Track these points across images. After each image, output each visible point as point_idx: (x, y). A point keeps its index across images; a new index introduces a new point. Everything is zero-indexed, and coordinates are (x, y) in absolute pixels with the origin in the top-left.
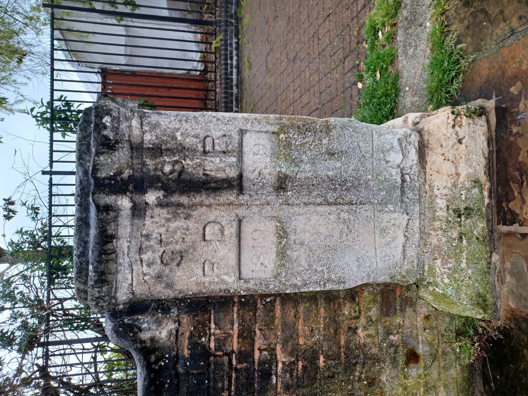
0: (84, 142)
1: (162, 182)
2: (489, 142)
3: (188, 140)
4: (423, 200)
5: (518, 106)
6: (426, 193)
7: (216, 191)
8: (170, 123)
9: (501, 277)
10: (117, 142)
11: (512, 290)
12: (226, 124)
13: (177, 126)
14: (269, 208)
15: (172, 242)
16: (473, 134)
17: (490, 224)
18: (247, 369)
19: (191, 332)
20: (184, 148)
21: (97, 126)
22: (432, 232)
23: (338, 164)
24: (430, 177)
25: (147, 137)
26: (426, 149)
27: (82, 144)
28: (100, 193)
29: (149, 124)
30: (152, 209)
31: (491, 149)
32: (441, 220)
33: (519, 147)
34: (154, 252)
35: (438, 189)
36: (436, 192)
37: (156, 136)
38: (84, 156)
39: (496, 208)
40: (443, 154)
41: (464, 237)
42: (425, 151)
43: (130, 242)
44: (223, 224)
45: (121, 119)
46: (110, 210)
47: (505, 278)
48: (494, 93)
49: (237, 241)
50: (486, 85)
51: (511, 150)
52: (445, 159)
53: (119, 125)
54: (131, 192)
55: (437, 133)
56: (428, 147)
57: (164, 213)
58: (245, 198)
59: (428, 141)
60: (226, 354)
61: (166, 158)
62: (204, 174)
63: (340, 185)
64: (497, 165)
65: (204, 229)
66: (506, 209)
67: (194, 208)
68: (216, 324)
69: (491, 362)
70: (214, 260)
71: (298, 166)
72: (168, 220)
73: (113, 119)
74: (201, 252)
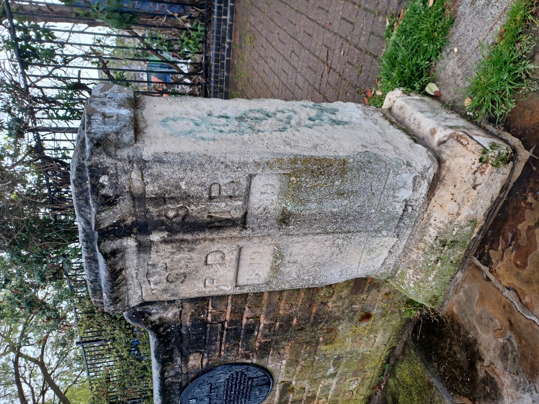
0: (81, 197)
1: (166, 225)
3: (193, 189)
4: (417, 225)
6: (423, 220)
7: (219, 229)
8: (173, 173)
9: (457, 289)
10: (117, 196)
11: (460, 303)
12: (235, 171)
13: (181, 176)
14: (269, 239)
16: (490, 182)
17: (468, 252)
18: (235, 329)
19: (192, 313)
20: (189, 196)
21: (93, 186)
22: (415, 249)
23: (346, 202)
24: (432, 208)
25: (149, 188)
26: (438, 183)
27: (79, 199)
28: (105, 241)
29: (151, 175)
30: (157, 246)
31: (501, 196)
32: (426, 244)
33: (524, 217)
34: (160, 275)
35: (435, 220)
36: (432, 221)
37: (159, 187)
38: (83, 209)
39: (479, 243)
40: (453, 194)
41: (440, 261)
42: (437, 184)
43: (137, 270)
44: (225, 252)
45: (120, 173)
46: (117, 253)
47: (459, 292)
48: (534, 147)
50: (532, 131)
51: (516, 213)
52: (452, 199)
53: (118, 180)
54: (136, 234)
55: (456, 172)
56: (442, 182)
57: (169, 248)
58: (248, 233)
59: (444, 176)
60: (220, 322)
61: (169, 205)
62: (208, 217)
65: (207, 257)
66: (486, 251)
67: (198, 242)
70: (214, 278)
71: (304, 205)
72: (173, 253)
73: (111, 176)
74: (203, 273)
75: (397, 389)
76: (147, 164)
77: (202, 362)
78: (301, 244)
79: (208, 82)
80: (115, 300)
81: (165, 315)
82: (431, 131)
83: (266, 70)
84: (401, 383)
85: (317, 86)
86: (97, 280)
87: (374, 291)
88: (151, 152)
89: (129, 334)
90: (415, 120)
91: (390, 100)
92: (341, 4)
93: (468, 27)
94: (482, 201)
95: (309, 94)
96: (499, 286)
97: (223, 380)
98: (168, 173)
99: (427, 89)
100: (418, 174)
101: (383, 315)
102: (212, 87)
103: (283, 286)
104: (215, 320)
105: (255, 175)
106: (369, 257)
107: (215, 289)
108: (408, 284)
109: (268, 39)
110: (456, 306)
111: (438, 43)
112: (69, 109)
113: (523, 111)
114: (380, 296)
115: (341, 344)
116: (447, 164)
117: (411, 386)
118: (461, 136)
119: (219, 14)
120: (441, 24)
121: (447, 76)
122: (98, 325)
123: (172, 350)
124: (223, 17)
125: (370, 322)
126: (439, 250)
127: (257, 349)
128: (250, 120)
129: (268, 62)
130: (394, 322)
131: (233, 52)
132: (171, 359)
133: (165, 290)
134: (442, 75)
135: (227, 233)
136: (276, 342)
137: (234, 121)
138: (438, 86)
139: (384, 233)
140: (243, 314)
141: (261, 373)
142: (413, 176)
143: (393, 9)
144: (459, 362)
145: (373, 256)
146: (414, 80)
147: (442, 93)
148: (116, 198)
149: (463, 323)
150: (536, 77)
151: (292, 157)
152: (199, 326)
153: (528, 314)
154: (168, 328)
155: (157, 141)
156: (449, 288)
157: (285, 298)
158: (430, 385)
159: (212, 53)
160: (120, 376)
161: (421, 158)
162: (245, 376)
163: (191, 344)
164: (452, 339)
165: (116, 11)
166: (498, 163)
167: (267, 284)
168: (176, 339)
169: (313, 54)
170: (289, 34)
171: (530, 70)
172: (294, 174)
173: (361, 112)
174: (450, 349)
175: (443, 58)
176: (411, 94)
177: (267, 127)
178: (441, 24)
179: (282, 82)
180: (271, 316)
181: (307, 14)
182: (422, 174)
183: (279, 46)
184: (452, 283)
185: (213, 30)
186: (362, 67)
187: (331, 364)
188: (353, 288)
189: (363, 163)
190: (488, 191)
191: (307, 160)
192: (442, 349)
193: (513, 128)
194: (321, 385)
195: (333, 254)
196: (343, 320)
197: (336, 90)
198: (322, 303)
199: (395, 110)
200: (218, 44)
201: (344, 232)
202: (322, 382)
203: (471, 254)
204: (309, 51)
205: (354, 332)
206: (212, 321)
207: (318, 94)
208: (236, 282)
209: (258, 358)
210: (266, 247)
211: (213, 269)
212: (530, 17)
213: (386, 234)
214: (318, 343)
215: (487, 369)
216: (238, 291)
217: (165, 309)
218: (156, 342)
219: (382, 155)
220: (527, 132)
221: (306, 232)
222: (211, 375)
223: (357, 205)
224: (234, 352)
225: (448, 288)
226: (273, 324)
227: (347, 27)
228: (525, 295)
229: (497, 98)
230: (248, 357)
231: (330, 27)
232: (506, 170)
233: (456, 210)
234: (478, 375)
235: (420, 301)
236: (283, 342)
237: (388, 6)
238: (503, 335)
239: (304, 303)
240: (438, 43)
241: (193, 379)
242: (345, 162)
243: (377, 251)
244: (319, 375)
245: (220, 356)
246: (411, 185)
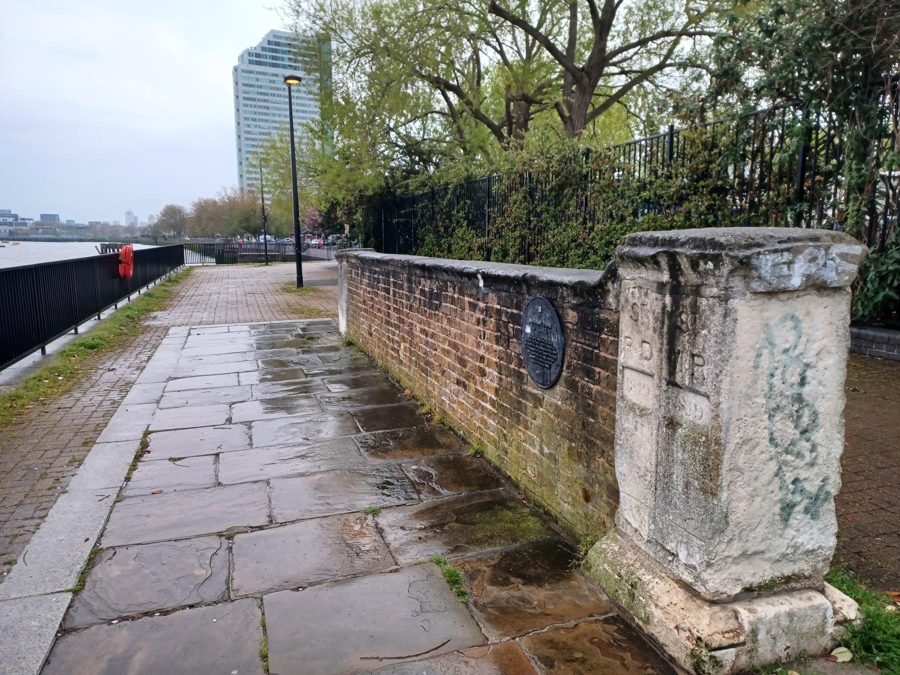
2: (672, 659)
10: (699, 273)
14: (657, 406)
23: (680, 489)
25: (704, 302)
30: (661, 300)
36: (657, 580)
57: (658, 310)
72: (654, 313)
80: (622, 257)
84: (523, 518)
88: (737, 307)
96: (581, 620)
101: (586, 515)
123: (582, 297)
125: (582, 500)
132: (576, 295)
133: (627, 300)
135: (665, 366)
141: (553, 378)
145: (634, 510)
151: (723, 441)
158: (515, 540)
164: (548, 571)
174: (540, 567)
180: (599, 397)
191: (718, 456)
195: (639, 468)
198: (604, 452)
208: (628, 368)
209: (566, 377)
214: (571, 441)
216: (620, 367)
224: (573, 355)
230: (568, 367)
233: (660, 604)
238: (539, 606)
241: (557, 312)
242: (714, 495)
244: (544, 436)
245: (573, 341)
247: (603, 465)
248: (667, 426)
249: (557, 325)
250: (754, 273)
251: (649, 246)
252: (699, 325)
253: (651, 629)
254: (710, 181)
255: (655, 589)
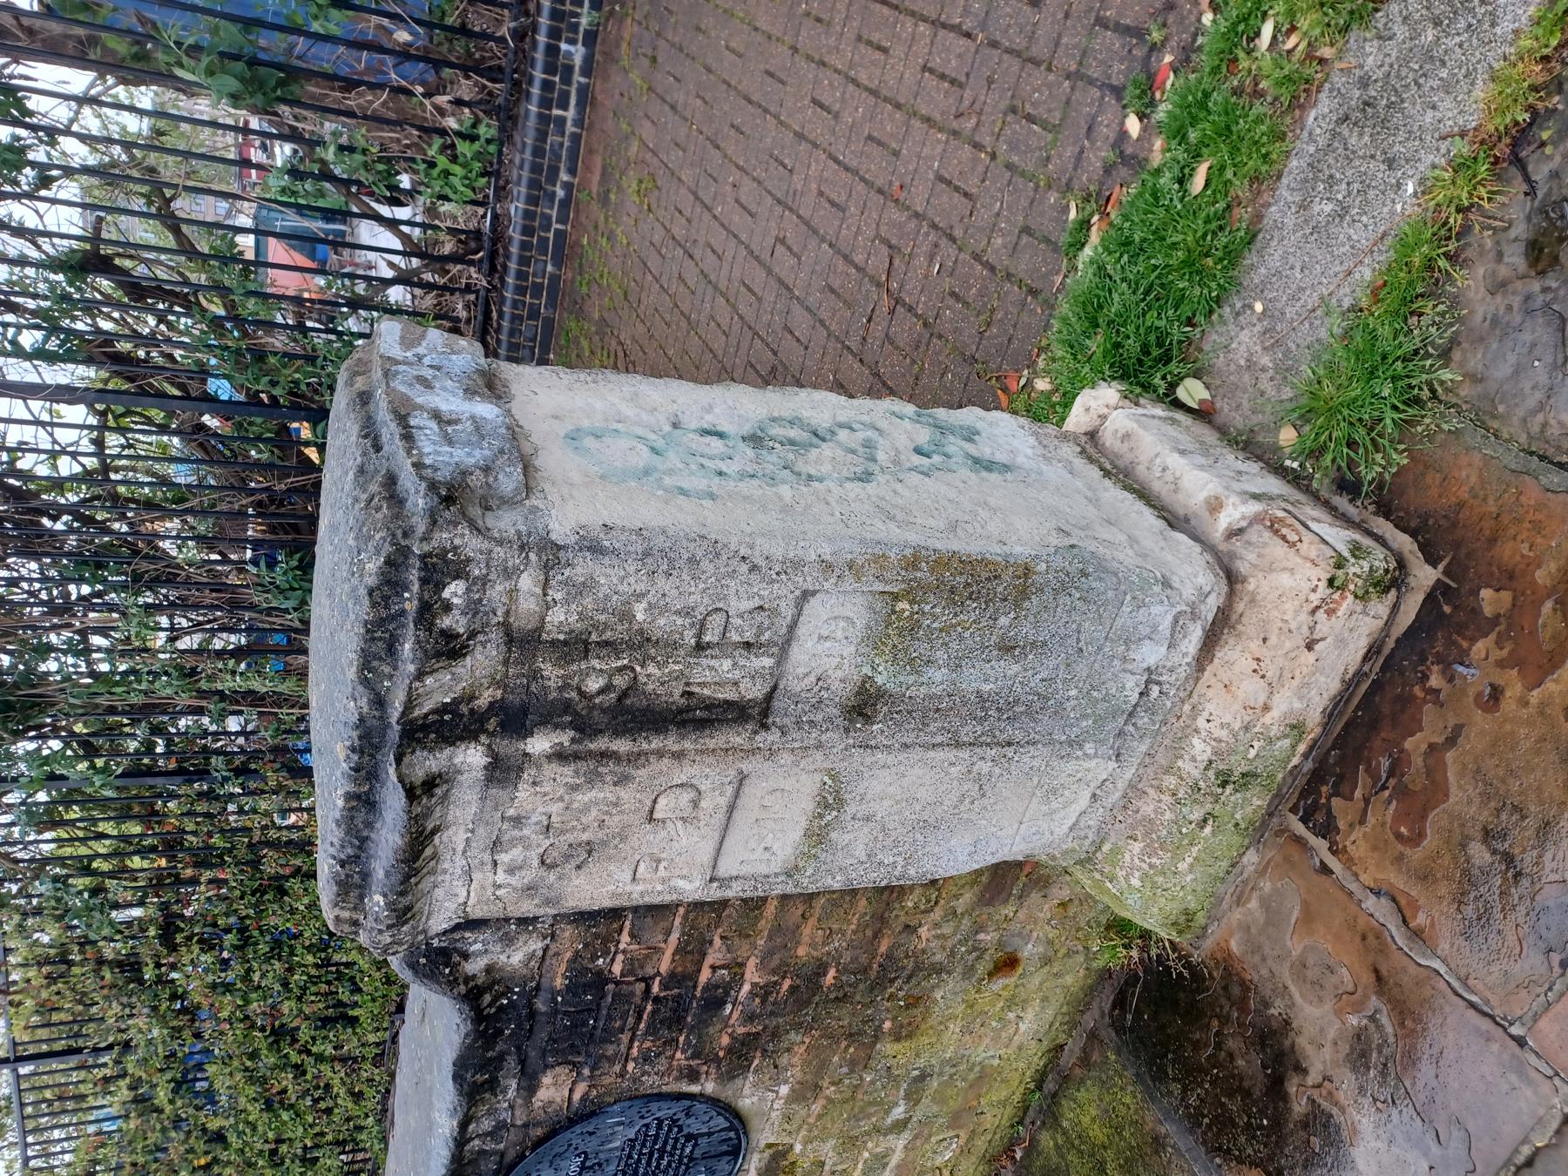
2: (1372, 651)
3: (662, 622)
5: (1473, 640)
6: (1179, 718)
9: (1242, 892)
10: (472, 635)
12: (773, 581)
13: (641, 587)
14: (819, 755)
15: (574, 828)
19: (577, 952)
20: (648, 640)
22: (1151, 792)
23: (1016, 668)
25: (557, 616)
27: (373, 639)
28: (413, 752)
30: (539, 767)
31: (1366, 668)
34: (527, 848)
36: (1201, 723)
38: (375, 663)
39: (1305, 780)
40: (1258, 660)
41: (1210, 822)
43: (472, 831)
44: (702, 788)
45: (493, 576)
47: (1249, 900)
49: (724, 821)
50: (1443, 522)
51: (1402, 711)
54: (491, 735)
58: (770, 738)
61: (596, 663)
63: (999, 710)
64: (1358, 708)
65: (655, 801)
66: (1323, 801)
68: (632, 935)
69: (1144, 989)
70: (663, 855)
72: (574, 788)
75: (1063, 1157)
76: (562, 554)
77: (571, 1091)
78: (894, 770)
79: (494, 287)
80: (402, 914)
81: (503, 958)
82: (1208, 502)
83: (686, 276)
85: (854, 343)
86: (358, 857)
87: (1035, 896)
89: (179, 1030)
90: (1164, 470)
91: (1088, 410)
92: (939, 141)
93: (1291, 259)
94: (1322, 679)
95: (827, 359)
97: (617, 1144)
98: (610, 579)
99: (1181, 393)
100: (1185, 608)
102: (508, 303)
103: (830, 881)
104: (631, 972)
105: (814, 593)
106: (1045, 808)
107: (659, 888)
108: (1126, 878)
109: (701, 194)
110: (1237, 936)
111: (1213, 285)
112: (54, 329)
113: (1423, 474)
114: (1046, 910)
115: (934, 1040)
116: (1251, 586)
117: (1105, 1148)
118: (1281, 520)
119: (545, 103)
120: (1223, 239)
121: (1232, 367)
122: (80, 1002)
123: (501, 1058)
124: (556, 112)
125: (1011, 980)
126: (1211, 794)
127: (721, 1054)
128: (777, 445)
129: (697, 257)
130: (1069, 980)
131: (577, 212)
132: (493, 1085)
133: (530, 889)
134: (1220, 361)
136: (775, 1035)
137: (741, 444)
138: (1208, 387)
139: (1089, 748)
140: (704, 955)
141: (721, 1122)
142: (1175, 611)
143: (1089, 180)
144: (1242, 1079)
145: (1054, 805)
146: (1148, 368)
147: (1218, 405)
148: (469, 639)
149: (1256, 979)
150: (1454, 400)
151: (908, 552)
152: (587, 987)
153: (1424, 955)
154: (503, 995)
155: (575, 494)
156: (1222, 890)
157: (817, 911)
159: (515, 208)
160: (134, 1165)
161: (1194, 575)
162: (680, 1129)
163: (555, 1041)
164: (1225, 1020)
165: (236, 57)
166: (1367, 592)
167: (789, 875)
168: (519, 1026)
169: (845, 257)
170: (769, 192)
171: (1442, 383)
172: (909, 595)
173: (1032, 440)
174: (1218, 1046)
175: (1224, 323)
176: (1142, 401)
177: (826, 468)
178: (1223, 239)
179: (741, 317)
180: (776, 961)
181: (833, 149)
182: (1193, 605)
183: (736, 218)
184: (1231, 878)
185: (524, 144)
186: (993, 310)
187: (902, 1093)
188: (987, 888)
189: (1068, 575)
190: (1339, 655)
191: (942, 562)
192: (1197, 1046)
193: (1397, 510)
194: (866, 1155)
196: (949, 973)
197: (914, 362)
198: (907, 926)
199: (1108, 438)
200: (534, 184)
201: (998, 744)
202: (870, 1145)
203: (1284, 808)
204: (831, 245)
205: (972, 1007)
206: (622, 975)
207: (857, 365)
210: (804, 777)
211: (663, 834)
212: (1442, 263)
213: (1092, 751)
215: (1315, 1094)
216: (714, 893)
217: (508, 940)
218: (467, 1035)
219: (1108, 557)
220: (1431, 522)
221: (908, 741)
222: (591, 1129)
223: (1038, 677)
224: (662, 1064)
225: (1221, 888)
226: (775, 983)
227: (947, 199)
228: (1417, 909)
229: (1360, 434)
230: (693, 1076)
231: (902, 196)
232: (1380, 608)
233: (1262, 699)
234: (1289, 1110)
235: (1149, 923)
236: (792, 1035)
237: (1075, 169)
238: (1357, 1008)
239: (862, 927)
240: (1213, 285)
241: (540, 1142)
243: (1066, 793)
244: (865, 1125)
246: (1168, 633)
247: (936, 925)
248: (868, 720)
249: (573, 1135)
250: (476, 480)
251: (369, 825)
252: (619, 632)
253: (1314, 719)
254: (146, 954)
255: (1227, 718)
